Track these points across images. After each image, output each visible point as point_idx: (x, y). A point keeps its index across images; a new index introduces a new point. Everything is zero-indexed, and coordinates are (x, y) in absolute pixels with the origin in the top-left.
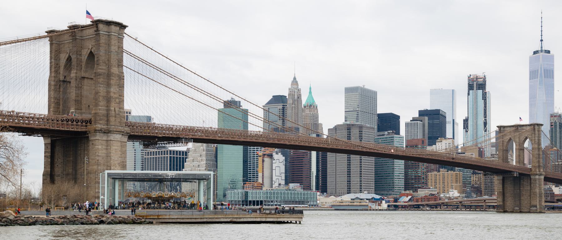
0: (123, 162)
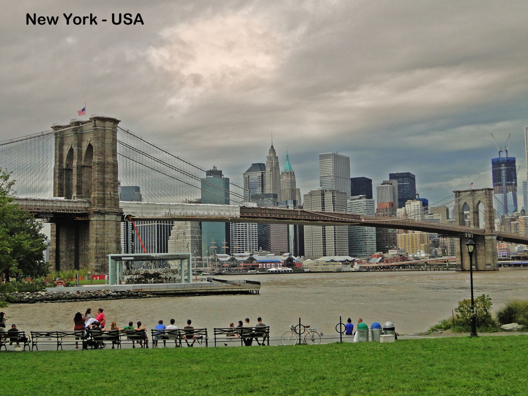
0: (118, 239)
